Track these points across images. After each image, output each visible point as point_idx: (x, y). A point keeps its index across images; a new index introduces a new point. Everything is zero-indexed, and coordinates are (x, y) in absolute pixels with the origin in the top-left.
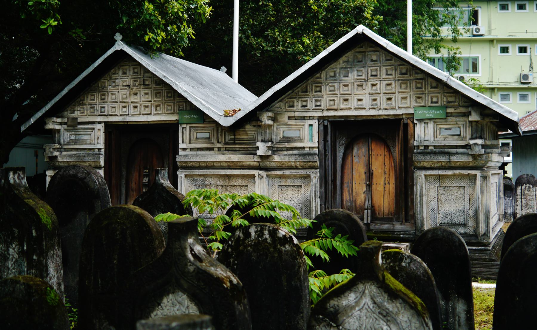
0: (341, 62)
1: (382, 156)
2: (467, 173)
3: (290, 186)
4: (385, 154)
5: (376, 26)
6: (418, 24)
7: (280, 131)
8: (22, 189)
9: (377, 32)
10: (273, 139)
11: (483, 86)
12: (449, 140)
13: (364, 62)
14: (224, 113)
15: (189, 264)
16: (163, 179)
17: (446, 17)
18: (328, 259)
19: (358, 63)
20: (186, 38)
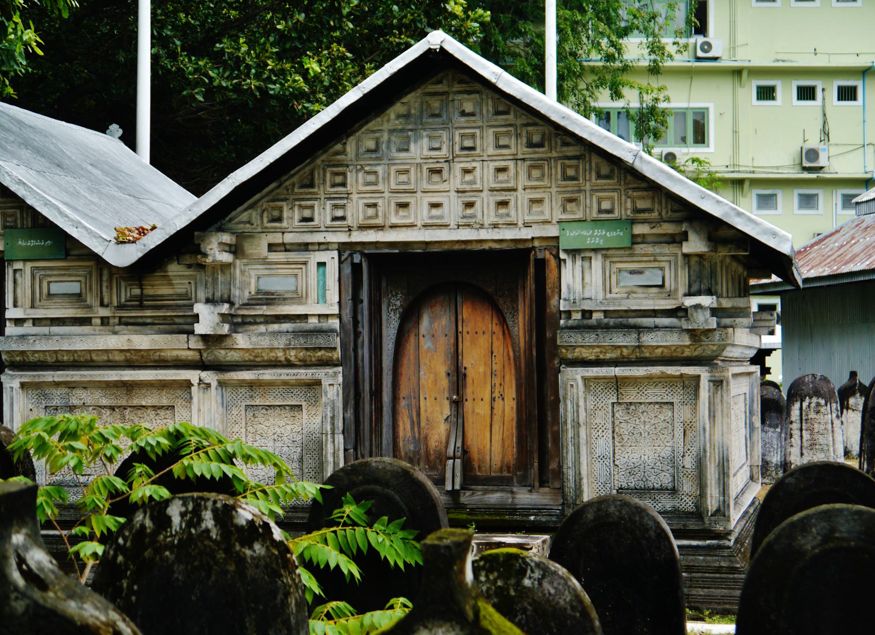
0: (393, 116)
1: (486, 336)
2: (678, 373)
3: (274, 406)
4: (494, 330)
5: (474, 33)
6: (572, 30)
7: (250, 277)
9: (479, 50)
10: (235, 296)
11: (718, 175)
12: (639, 298)
13: (445, 117)
14: (115, 234)
17: (635, 16)
18: (357, 575)
19: (430, 120)
20: (20, 54)
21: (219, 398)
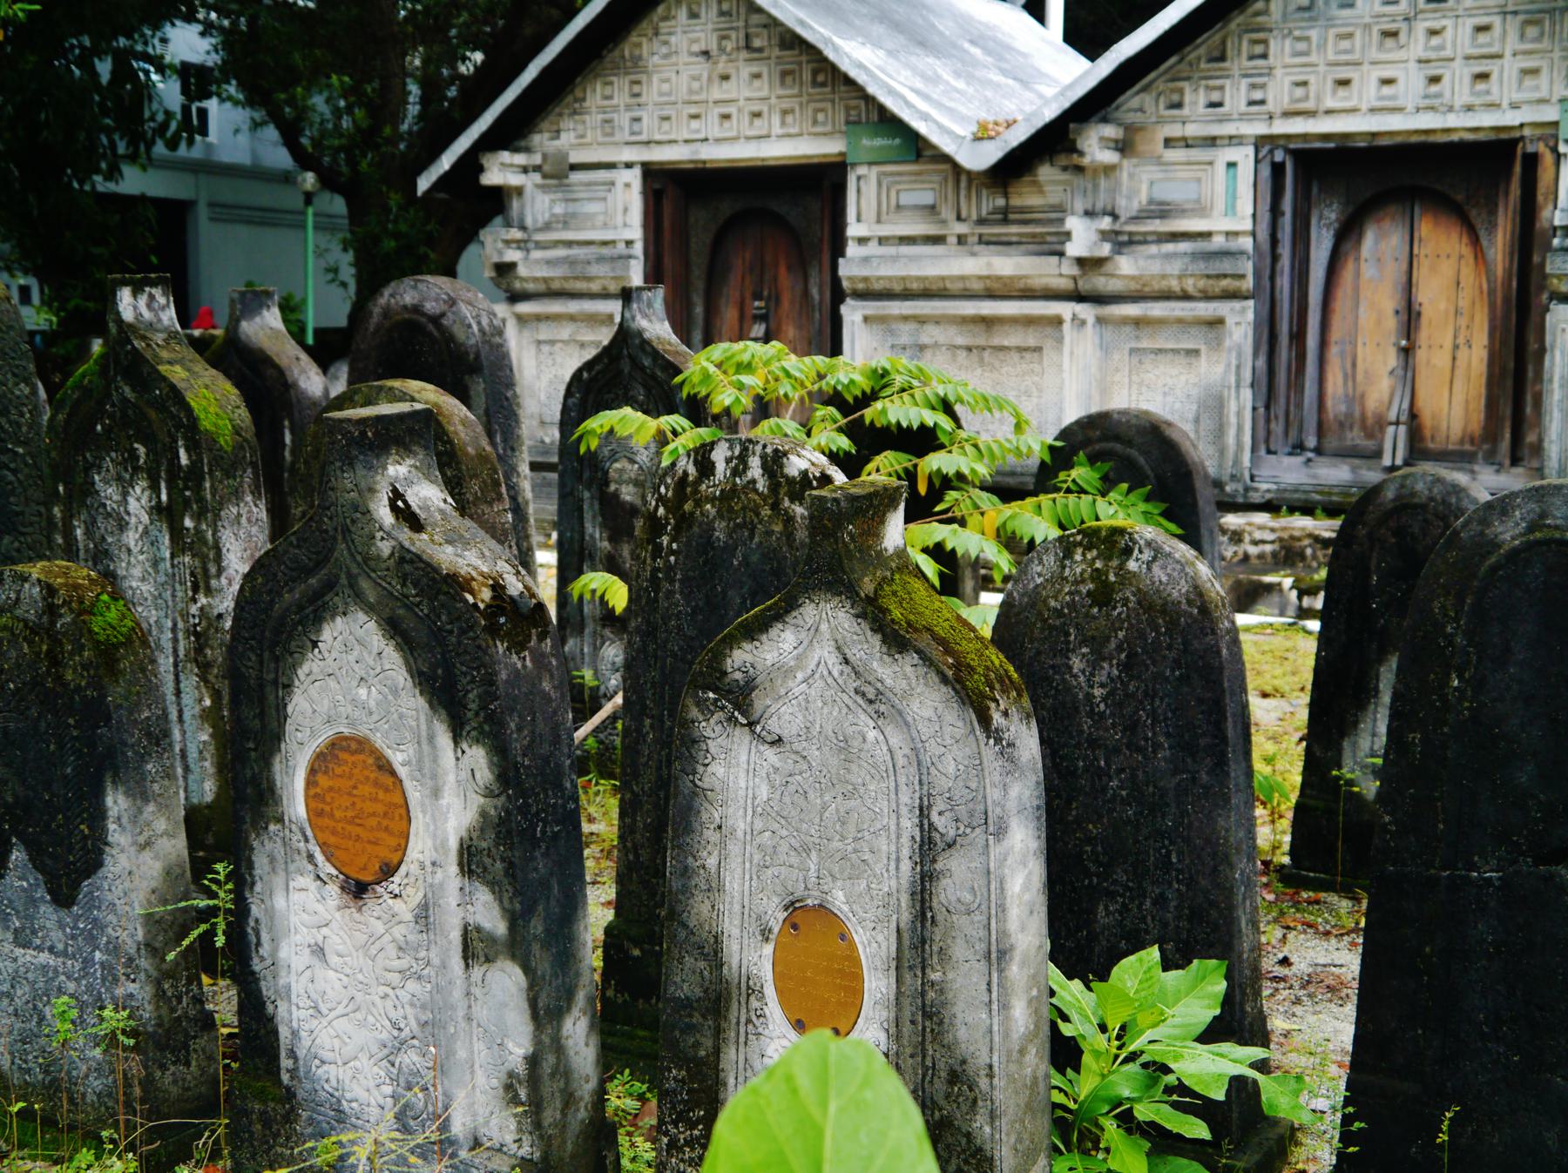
8: (159, 338)
15: (379, 535)
16: (645, 316)
21: (1097, 341)
